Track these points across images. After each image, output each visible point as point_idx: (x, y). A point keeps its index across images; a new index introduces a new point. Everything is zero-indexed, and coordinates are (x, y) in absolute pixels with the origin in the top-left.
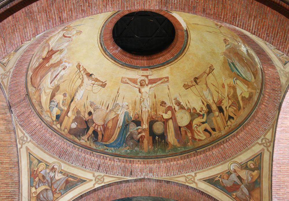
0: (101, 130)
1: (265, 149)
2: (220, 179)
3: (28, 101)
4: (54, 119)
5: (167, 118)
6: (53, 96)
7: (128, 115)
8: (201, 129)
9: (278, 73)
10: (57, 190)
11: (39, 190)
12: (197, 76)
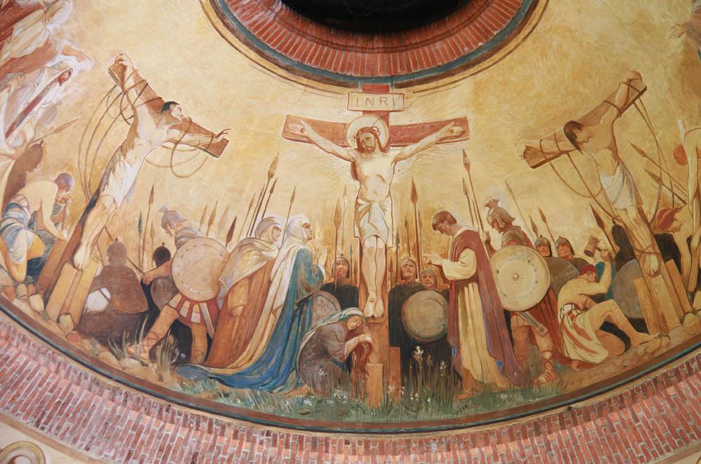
0: (203, 321)
4: (21, 274)
5: (458, 276)
7: (310, 264)
12: (576, 119)
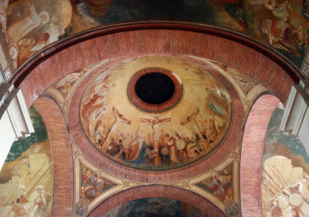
0: (127, 152)
1: (235, 160)
2: (205, 183)
3: (81, 127)
4: (97, 142)
5: (170, 145)
6: (97, 127)
7: (145, 143)
9: (242, 103)
10: (99, 189)
11: (87, 189)
12: (189, 117)
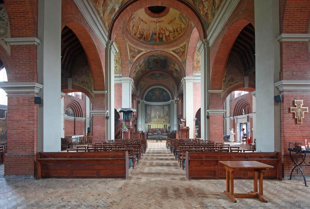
6: (133, 27)
8: (172, 37)
